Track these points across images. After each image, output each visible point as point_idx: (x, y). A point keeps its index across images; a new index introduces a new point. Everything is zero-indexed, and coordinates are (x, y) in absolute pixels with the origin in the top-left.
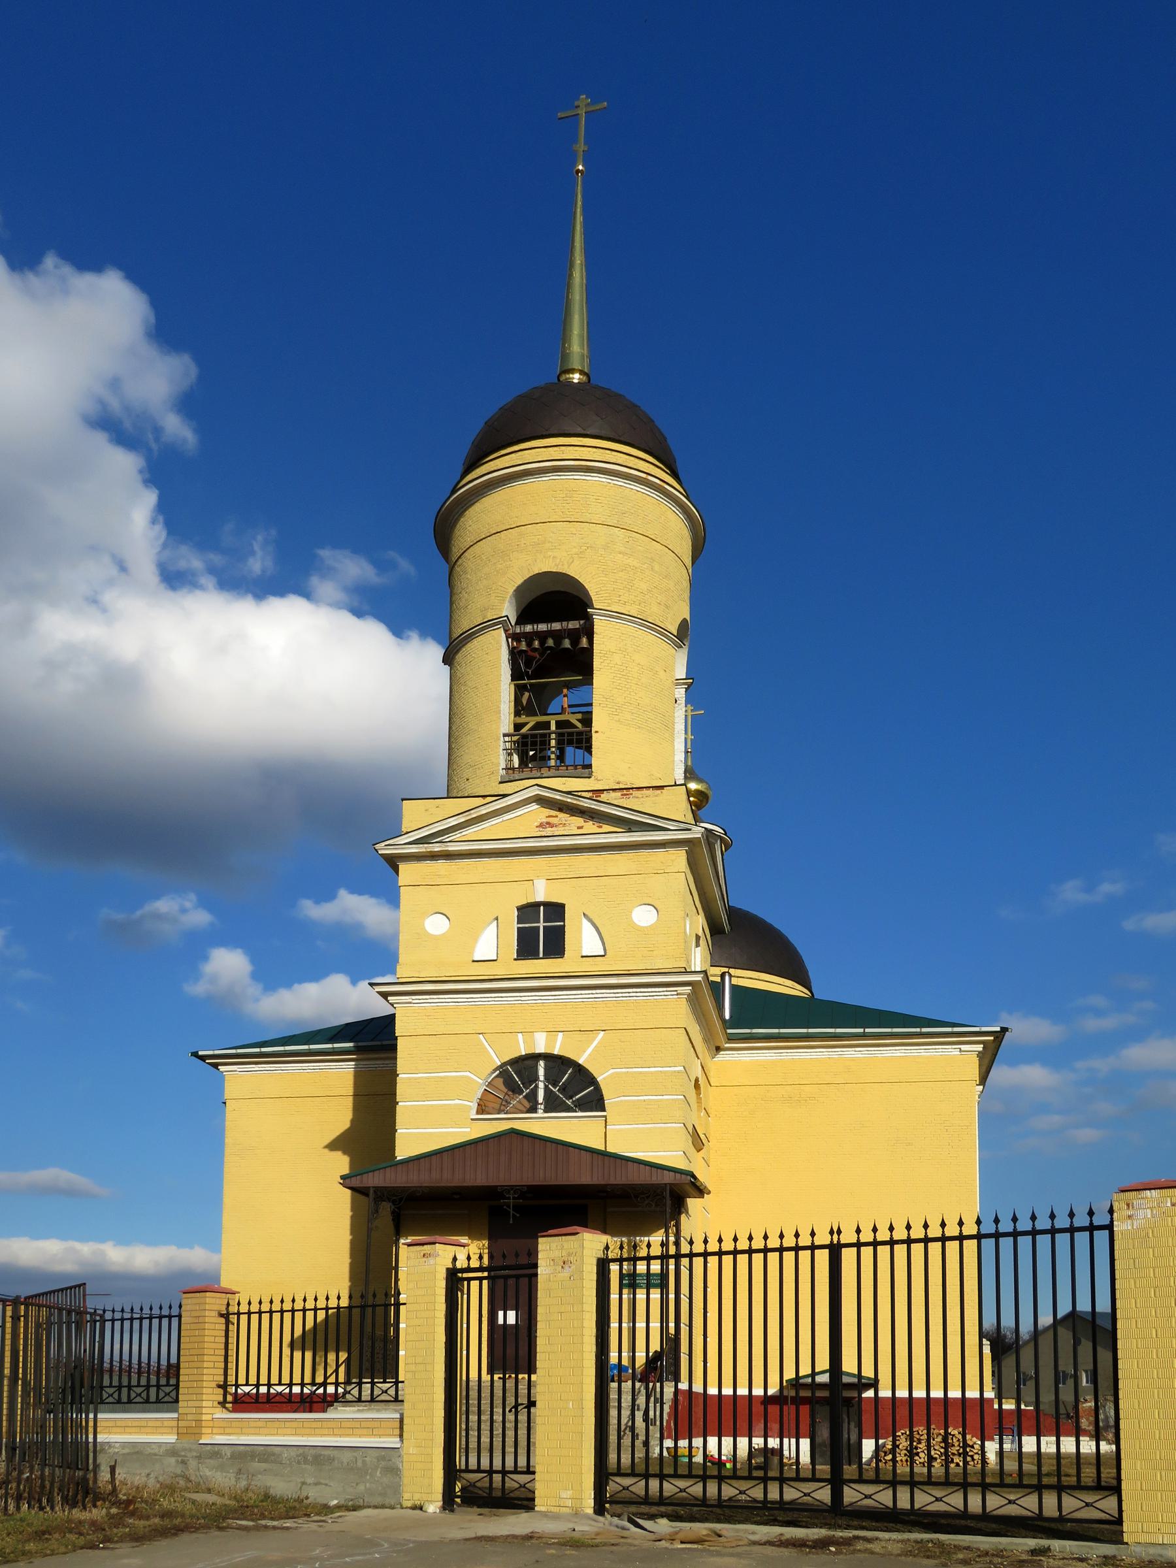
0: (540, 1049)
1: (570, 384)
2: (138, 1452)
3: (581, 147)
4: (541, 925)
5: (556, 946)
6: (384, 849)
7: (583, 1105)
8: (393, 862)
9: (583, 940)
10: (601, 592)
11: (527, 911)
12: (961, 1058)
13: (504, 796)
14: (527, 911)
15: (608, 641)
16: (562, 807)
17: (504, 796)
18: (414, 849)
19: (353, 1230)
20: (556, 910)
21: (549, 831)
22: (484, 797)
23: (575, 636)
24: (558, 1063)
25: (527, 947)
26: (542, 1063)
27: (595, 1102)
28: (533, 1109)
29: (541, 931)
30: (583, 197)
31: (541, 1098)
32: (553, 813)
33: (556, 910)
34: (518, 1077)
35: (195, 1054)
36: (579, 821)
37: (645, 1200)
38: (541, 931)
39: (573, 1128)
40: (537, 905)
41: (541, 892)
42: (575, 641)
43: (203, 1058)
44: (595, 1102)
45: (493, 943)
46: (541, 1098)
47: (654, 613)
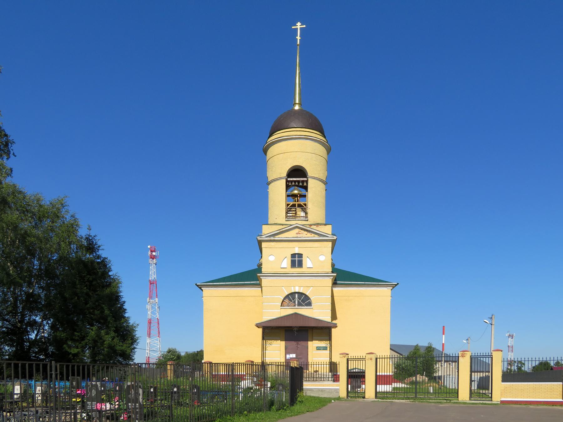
0: (297, 291)
1: (296, 111)
2: (311, 390)
4: (297, 259)
5: (300, 265)
6: (259, 238)
9: (307, 263)
10: (310, 172)
11: (293, 256)
12: (386, 292)
13: (291, 225)
14: (293, 256)
15: (312, 184)
16: (302, 229)
17: (291, 225)
18: (267, 239)
20: (300, 255)
21: (299, 236)
22: (283, 225)
24: (300, 294)
25: (293, 264)
27: (310, 304)
28: (295, 306)
29: (297, 260)
31: (297, 303)
33: (300, 255)
34: (291, 298)
36: (306, 233)
37: (323, 331)
38: (297, 260)
39: (304, 311)
40: (296, 254)
41: (297, 251)
42: (303, 184)
44: (310, 304)
45: (286, 263)
46: (297, 303)
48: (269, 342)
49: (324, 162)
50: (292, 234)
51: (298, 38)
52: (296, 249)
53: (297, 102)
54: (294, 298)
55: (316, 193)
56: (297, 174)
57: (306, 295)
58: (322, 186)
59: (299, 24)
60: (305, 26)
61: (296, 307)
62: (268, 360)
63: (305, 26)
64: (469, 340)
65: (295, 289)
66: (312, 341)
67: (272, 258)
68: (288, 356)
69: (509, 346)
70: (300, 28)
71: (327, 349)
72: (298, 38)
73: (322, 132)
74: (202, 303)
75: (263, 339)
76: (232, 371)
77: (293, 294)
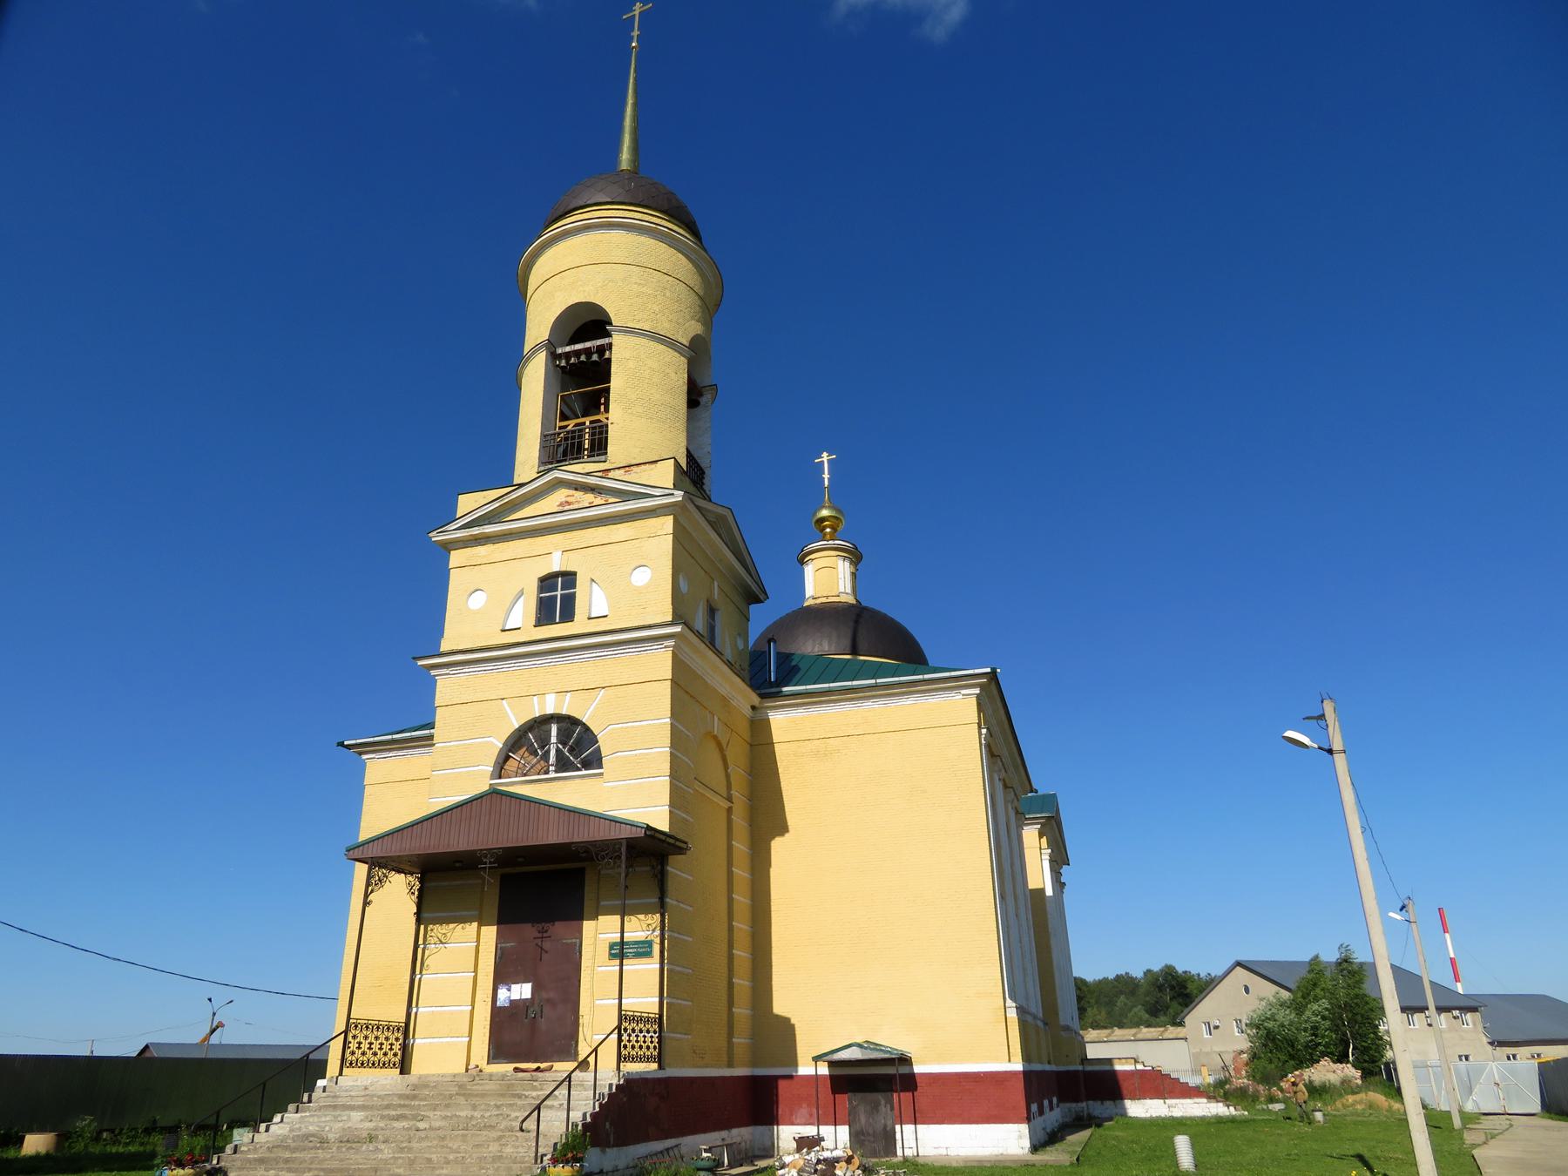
3: (636, 33)
4: (559, 593)
7: (587, 765)
8: (448, 547)
11: (547, 582)
18: (459, 534)
19: (966, 1160)
20: (569, 578)
23: (601, 350)
24: (568, 723)
25: (545, 613)
26: (554, 729)
27: (594, 761)
28: (547, 772)
30: (636, 105)
31: (552, 759)
32: (572, 492)
33: (569, 578)
35: (341, 744)
41: (556, 564)
43: (349, 747)
44: (594, 761)
45: (522, 615)
46: (552, 759)
47: (665, 328)
48: (437, 930)
49: (689, 300)
52: (554, 555)
54: (545, 742)
56: (588, 324)
57: (587, 729)
62: (628, 937)
64: (1410, 907)
65: (542, 704)
66: (594, 917)
67: (477, 601)
68: (503, 994)
71: (648, 954)
73: (695, 233)
74: (361, 789)
75: (419, 921)
76: (663, 921)
77: (539, 725)
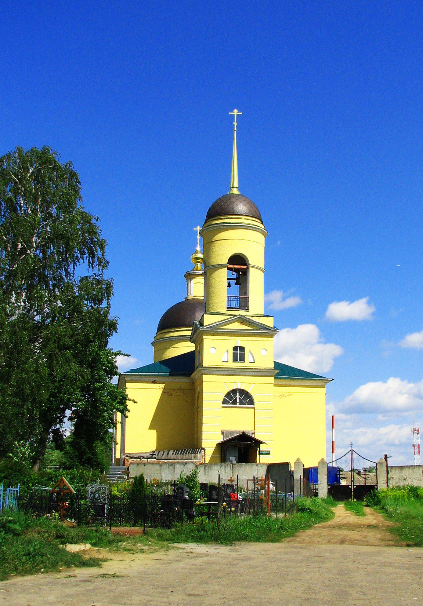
5: (242, 359)
10: (252, 261)
11: (235, 349)
14: (235, 349)
20: (242, 349)
29: (239, 353)
38: (239, 353)
46: (238, 401)
50: (236, 326)
51: (235, 124)
53: (236, 185)
55: (256, 280)
58: (262, 274)
59: (236, 111)
60: (230, 113)
61: (238, 405)
63: (230, 113)
69: (414, 446)
70: (237, 115)
72: (235, 124)
77: (234, 391)
